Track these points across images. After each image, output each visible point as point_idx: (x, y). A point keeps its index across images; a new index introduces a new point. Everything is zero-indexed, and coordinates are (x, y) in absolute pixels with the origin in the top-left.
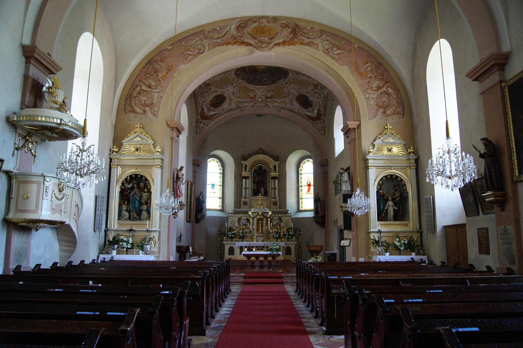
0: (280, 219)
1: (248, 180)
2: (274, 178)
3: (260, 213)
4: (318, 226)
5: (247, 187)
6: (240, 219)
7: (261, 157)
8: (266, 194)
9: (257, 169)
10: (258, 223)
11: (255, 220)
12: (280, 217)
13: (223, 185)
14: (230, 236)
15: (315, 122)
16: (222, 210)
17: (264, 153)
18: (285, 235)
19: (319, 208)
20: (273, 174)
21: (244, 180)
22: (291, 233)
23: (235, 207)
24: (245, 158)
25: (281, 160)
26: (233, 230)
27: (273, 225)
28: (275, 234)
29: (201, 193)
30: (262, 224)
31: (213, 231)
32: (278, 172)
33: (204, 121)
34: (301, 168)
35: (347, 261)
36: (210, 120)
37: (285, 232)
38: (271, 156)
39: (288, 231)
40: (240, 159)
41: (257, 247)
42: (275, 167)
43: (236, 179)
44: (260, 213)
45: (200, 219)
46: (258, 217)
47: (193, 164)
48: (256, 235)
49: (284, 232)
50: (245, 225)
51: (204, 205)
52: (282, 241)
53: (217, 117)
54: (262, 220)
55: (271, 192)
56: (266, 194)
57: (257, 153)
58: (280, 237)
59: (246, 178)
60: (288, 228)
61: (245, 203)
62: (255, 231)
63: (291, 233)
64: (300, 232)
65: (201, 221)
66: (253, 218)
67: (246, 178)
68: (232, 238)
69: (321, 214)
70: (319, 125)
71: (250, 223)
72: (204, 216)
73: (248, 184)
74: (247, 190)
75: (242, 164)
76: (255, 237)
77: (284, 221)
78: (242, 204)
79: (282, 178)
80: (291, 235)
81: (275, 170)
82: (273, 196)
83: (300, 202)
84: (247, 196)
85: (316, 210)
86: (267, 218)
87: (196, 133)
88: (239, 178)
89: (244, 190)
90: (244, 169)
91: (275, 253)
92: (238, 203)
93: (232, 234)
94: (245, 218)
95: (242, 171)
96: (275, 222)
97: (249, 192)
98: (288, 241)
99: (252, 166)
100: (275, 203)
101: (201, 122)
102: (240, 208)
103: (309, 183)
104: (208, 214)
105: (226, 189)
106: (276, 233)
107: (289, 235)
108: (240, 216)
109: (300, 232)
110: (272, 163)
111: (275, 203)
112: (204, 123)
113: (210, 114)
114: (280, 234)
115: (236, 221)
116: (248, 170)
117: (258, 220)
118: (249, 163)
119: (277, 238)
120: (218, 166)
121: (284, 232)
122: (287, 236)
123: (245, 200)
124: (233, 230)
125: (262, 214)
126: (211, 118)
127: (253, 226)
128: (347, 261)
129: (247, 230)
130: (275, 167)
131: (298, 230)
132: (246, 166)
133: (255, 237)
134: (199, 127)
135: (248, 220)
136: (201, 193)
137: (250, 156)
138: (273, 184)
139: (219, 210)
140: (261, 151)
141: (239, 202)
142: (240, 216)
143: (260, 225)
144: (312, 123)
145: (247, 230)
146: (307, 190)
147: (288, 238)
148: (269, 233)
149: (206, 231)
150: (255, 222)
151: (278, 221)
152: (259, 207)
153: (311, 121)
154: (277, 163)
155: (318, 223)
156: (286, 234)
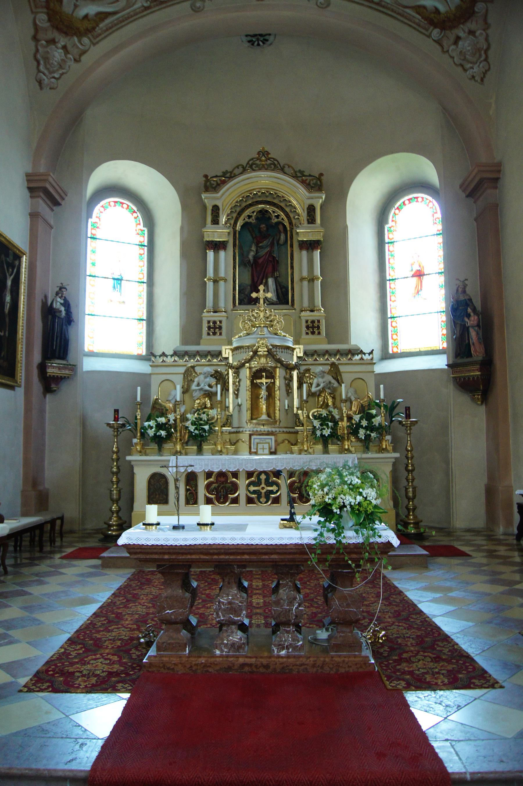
0: (335, 372)
1: (222, 253)
2: (310, 246)
3: (262, 351)
4: (464, 399)
5: (222, 274)
6: (189, 375)
7: (263, 180)
8: (283, 298)
9: (252, 220)
10: (255, 387)
11: (246, 373)
12: (333, 365)
13: (150, 282)
14: (151, 433)
15: (451, 35)
16: (150, 355)
17: (275, 166)
18: (354, 430)
19: (473, 334)
20: (304, 232)
21: (211, 254)
22: (377, 421)
23: (185, 341)
24: (212, 185)
25: (329, 187)
26: (163, 413)
27: (311, 394)
28: (317, 423)
29: (62, 288)
30: (270, 389)
31: (102, 417)
32: (322, 224)
33: (62, 41)
34: (390, 223)
35: (84, 370)
36: (85, 40)
37: (357, 418)
38: (299, 176)
39: (365, 412)
40: (199, 189)
41: (250, 474)
42: (311, 210)
43: (185, 254)
44: (262, 351)
45: (59, 379)
46: (255, 364)
47: (31, 189)
48: (249, 428)
49: (350, 418)
50: (211, 395)
51: (71, 331)
52: (343, 450)
53: (111, 29)
54: (271, 375)
55: (300, 292)
56: (283, 298)
57: (252, 166)
58: (335, 436)
59: (217, 246)
60: (364, 401)
61: (215, 328)
62: (246, 415)
63: (377, 421)
64: (408, 416)
65: (65, 388)
66: (237, 370)
67: (217, 246)
68: (159, 441)
69: (478, 352)
70: (465, 45)
71: (225, 388)
72: (73, 368)
73: (223, 264)
74: (222, 283)
75: (205, 207)
76: (245, 437)
77: (347, 378)
78: (205, 329)
79: (331, 247)
80: (380, 429)
81: (311, 220)
82: (306, 304)
83: (390, 328)
84: (222, 305)
85: (460, 345)
86: (289, 368)
87: (40, 82)
88: (197, 249)
89: (210, 286)
90: (209, 219)
91: (351, 537)
92: (191, 331)
93: (160, 426)
94: (210, 370)
95: (204, 225)
96: (317, 383)
97: (226, 292)
98: (367, 449)
99: (238, 211)
100: (313, 327)
101: (52, 42)
102: (199, 344)
103: (416, 268)
104: (89, 365)
105: (158, 290)
106: (323, 420)
107: (371, 428)
108: (192, 363)
109: (408, 416)
110: (298, 197)
111: (313, 327)
112: (64, 47)
113: (82, 12)
114: (336, 423)
115: (179, 381)
116: (223, 219)
117: (256, 375)
118: (227, 197)
119: (325, 441)
120: (133, 222)
121: (350, 418)
122: (362, 433)
123: (216, 317)
124: (163, 413)
125: (270, 354)
126: (88, 31)
127: (236, 399)
128: (84, 370)
129: (213, 413)
130: (311, 210)
131: (401, 409)
132: (216, 209)
133: (245, 437)
134: (46, 59)
135: (220, 378)
136: (62, 288)
137: (228, 176)
138: (304, 265)
139: (140, 358)
140: (264, 161)
141: (200, 326)
142: (192, 363)
143: (263, 393)
144: (438, 42)
145: (213, 413)
146: (413, 290)
147: (368, 437)
148: (297, 421)
149: (84, 422)
150: (246, 383)
151: (329, 378)
152: (260, 330)
153: (436, 33)
154: (319, 200)
155: (465, 385)
156: (359, 425)
